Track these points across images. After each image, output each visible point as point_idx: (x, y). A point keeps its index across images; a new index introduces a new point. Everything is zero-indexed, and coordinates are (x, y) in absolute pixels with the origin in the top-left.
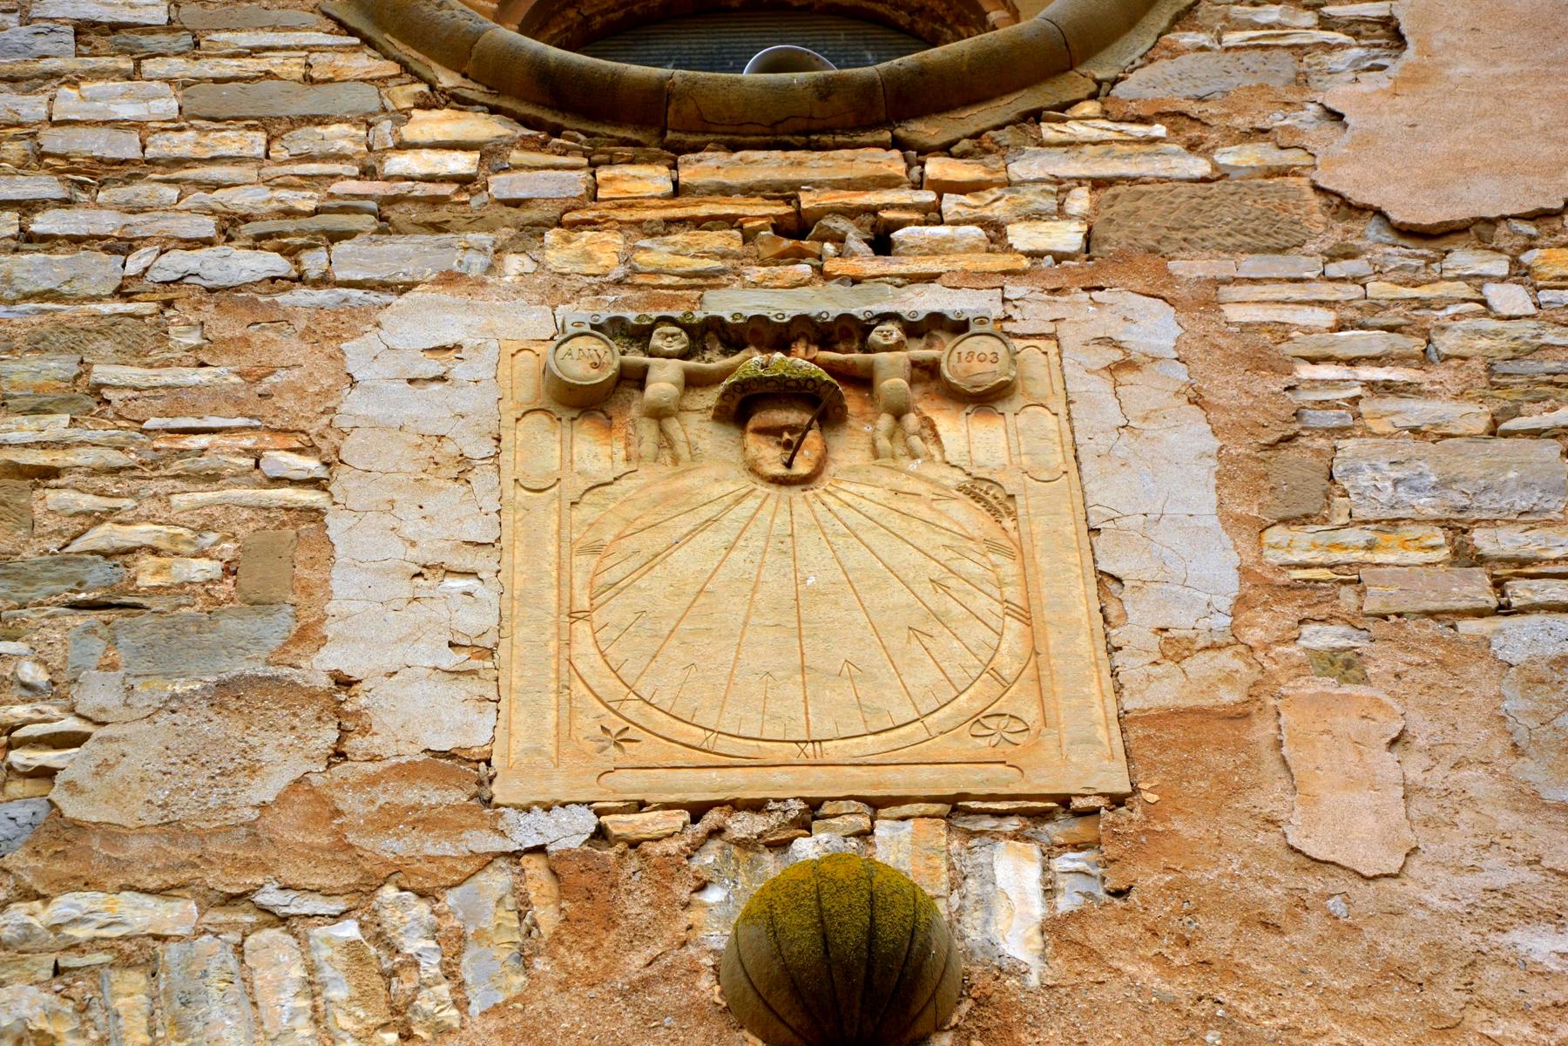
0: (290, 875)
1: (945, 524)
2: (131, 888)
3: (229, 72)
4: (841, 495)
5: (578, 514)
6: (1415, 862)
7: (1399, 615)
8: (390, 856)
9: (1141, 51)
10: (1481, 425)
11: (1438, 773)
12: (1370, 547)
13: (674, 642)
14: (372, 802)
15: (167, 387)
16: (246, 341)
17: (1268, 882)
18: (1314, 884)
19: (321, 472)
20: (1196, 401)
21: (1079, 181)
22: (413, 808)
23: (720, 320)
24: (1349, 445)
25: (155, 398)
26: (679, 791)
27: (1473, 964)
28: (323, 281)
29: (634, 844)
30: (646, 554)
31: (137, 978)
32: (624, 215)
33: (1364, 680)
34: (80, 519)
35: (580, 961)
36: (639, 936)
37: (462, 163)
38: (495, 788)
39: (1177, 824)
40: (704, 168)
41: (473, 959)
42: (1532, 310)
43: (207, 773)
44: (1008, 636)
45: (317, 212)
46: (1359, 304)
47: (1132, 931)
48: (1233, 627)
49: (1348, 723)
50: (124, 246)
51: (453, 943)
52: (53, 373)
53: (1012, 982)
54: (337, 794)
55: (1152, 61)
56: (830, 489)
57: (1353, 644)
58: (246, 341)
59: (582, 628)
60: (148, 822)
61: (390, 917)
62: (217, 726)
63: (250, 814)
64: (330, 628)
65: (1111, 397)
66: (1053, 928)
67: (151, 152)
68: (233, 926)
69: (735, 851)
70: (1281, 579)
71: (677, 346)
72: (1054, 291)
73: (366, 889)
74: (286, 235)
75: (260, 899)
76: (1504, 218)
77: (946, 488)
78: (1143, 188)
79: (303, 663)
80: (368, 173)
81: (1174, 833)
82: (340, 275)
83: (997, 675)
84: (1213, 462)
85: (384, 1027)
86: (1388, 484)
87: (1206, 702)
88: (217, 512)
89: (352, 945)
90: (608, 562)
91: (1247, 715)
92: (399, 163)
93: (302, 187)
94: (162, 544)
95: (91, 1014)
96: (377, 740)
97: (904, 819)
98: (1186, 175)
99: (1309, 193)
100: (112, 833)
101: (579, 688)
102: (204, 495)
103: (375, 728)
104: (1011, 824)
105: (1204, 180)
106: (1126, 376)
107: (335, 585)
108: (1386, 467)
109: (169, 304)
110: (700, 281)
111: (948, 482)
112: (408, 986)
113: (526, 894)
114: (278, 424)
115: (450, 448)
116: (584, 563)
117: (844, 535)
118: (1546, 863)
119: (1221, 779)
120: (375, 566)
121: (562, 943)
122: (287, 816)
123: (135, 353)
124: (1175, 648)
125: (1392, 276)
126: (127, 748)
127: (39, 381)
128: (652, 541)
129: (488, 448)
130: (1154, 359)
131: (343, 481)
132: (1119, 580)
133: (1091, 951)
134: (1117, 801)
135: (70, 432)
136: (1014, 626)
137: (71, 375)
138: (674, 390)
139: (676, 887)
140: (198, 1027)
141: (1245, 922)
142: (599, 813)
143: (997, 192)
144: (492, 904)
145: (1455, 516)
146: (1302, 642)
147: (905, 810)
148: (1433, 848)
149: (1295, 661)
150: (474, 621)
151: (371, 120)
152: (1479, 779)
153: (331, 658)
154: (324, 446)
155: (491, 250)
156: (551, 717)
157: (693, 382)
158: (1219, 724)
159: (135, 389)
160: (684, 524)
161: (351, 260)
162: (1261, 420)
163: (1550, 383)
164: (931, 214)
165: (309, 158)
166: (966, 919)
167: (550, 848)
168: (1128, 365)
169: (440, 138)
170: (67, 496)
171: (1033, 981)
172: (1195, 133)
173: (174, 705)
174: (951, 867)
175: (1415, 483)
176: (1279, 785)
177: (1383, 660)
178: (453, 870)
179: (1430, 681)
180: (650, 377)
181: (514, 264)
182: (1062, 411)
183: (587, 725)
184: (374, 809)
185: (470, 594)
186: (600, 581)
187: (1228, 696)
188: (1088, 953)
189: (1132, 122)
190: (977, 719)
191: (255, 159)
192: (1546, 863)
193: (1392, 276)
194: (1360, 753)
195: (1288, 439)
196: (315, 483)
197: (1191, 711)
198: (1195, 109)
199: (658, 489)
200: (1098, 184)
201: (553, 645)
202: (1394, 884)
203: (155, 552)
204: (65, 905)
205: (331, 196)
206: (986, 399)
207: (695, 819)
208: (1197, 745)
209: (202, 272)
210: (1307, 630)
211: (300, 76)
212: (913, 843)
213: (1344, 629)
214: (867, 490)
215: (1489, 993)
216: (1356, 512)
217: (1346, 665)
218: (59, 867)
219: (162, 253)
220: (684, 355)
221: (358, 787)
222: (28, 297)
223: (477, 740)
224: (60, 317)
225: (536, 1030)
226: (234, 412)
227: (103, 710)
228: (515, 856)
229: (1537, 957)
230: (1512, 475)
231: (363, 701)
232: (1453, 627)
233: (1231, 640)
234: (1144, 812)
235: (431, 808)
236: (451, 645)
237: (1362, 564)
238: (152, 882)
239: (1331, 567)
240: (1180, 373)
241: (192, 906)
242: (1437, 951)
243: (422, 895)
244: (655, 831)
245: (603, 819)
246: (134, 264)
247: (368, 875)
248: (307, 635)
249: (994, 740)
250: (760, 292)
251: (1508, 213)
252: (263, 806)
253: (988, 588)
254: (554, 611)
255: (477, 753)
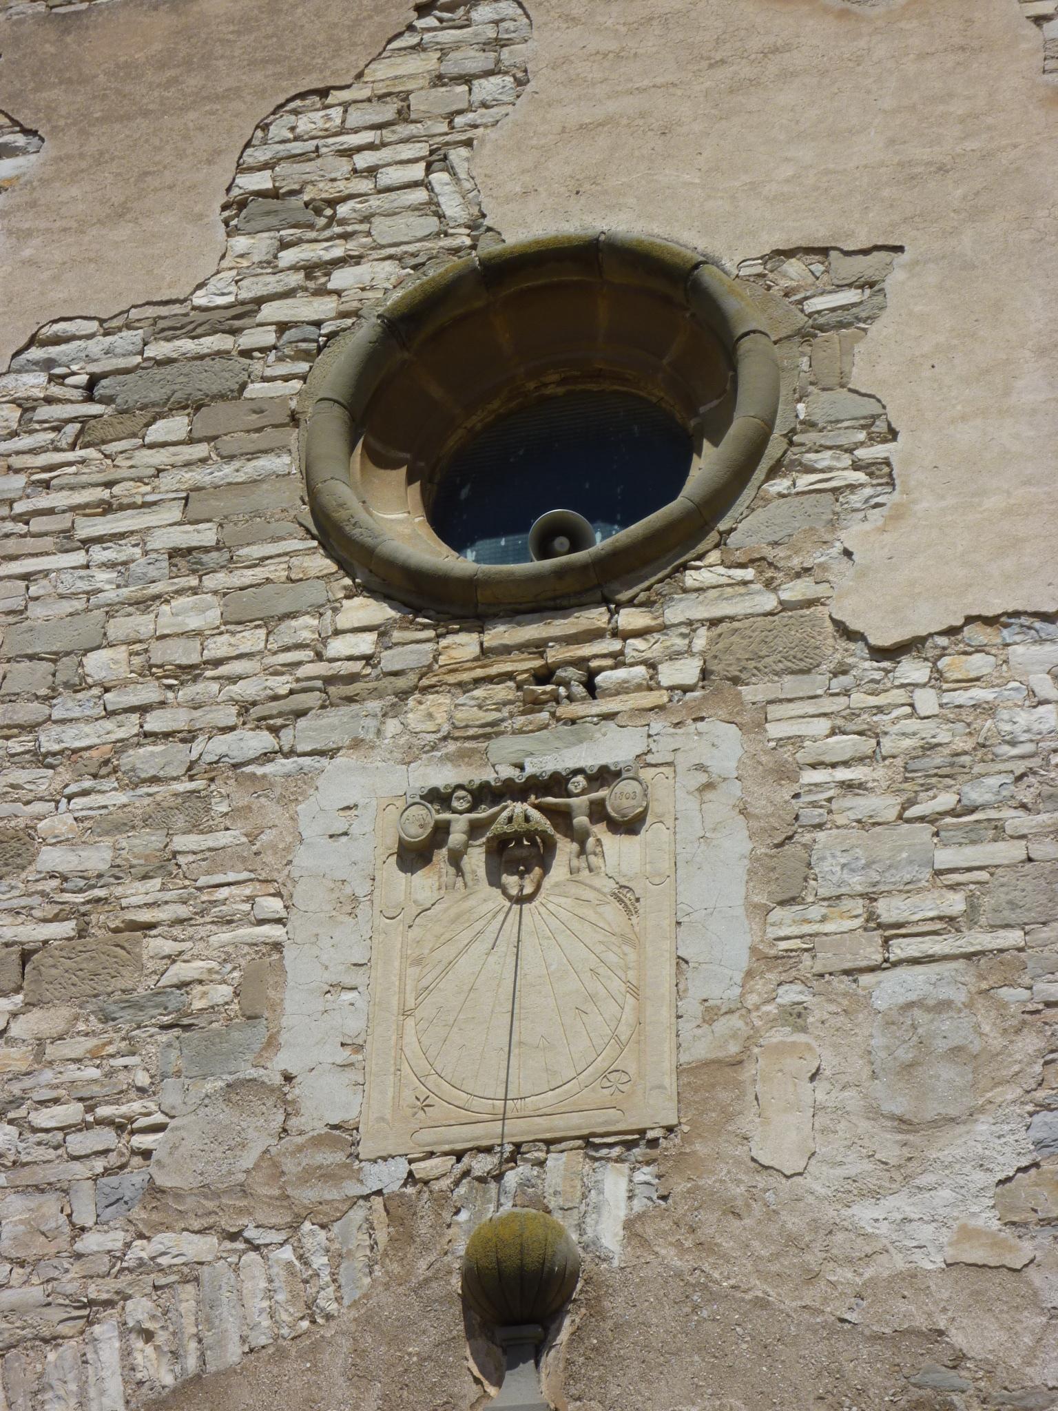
0: (261, 1217)
1: (601, 925)
2: (187, 1230)
3: (247, 581)
4: (550, 906)
5: (411, 934)
6: (813, 1161)
7: (831, 974)
8: (306, 1202)
9: (746, 504)
10: (892, 814)
11: (834, 1094)
12: (824, 919)
13: (455, 1029)
14: (299, 1164)
15: (210, 850)
16: (249, 808)
17: (738, 1182)
18: (761, 1180)
19: (283, 914)
20: (743, 812)
21: (702, 622)
22: (320, 1167)
23: (488, 783)
24: (821, 836)
25: (204, 860)
26: (451, 1142)
27: (830, 1232)
28: (291, 753)
29: (426, 1183)
30: (445, 962)
31: (190, 1288)
32: (451, 679)
33: (804, 1029)
34: (165, 961)
35: (395, 1268)
36: (426, 1248)
37: (365, 644)
38: (360, 1149)
39: (698, 1147)
40: (499, 634)
41: (346, 1269)
42: (936, 710)
43: (222, 1149)
44: (627, 1009)
45: (292, 692)
46: (844, 713)
47: (666, 1225)
48: (742, 995)
49: (791, 1063)
50: (189, 737)
51: (337, 1258)
52: (153, 846)
53: (604, 1266)
54: (283, 1160)
55: (753, 510)
56: (544, 901)
57: (805, 999)
58: (249, 808)
59: (410, 1022)
60: (195, 1185)
61: (308, 1243)
62: (224, 1114)
63: (241, 1177)
64: (283, 1037)
65: (697, 813)
66: (629, 1225)
67: (207, 655)
68: (234, 1251)
69: (476, 1184)
70: (773, 952)
71: (466, 805)
72: (676, 725)
73: (294, 1227)
74: (271, 717)
75: (246, 1234)
76: (931, 635)
77: (604, 895)
78: (736, 624)
79: (269, 1065)
80: (319, 656)
81: (694, 1152)
82: (300, 749)
83: (619, 1042)
84: (746, 862)
85: (302, 1318)
86: (838, 868)
87: (720, 1054)
88: (230, 949)
89: (289, 1264)
90: (425, 971)
91: (741, 1062)
92: (338, 647)
93: (282, 674)
94: (204, 977)
95: (170, 1315)
96: (303, 1120)
97: (562, 1152)
98: (761, 611)
99: (828, 623)
100: (178, 1195)
101: (405, 1067)
102: (225, 935)
103: (302, 1111)
104: (616, 1151)
105: (771, 614)
106: (709, 795)
107: (287, 1004)
108: (839, 854)
109: (212, 780)
110: (488, 730)
111: (606, 890)
112: (314, 1290)
113: (371, 1223)
114: (263, 876)
115: (348, 890)
116: (413, 972)
117: (548, 938)
118: (877, 1156)
119: (723, 1110)
120: (306, 987)
121: (387, 1255)
122: (258, 1177)
123: (195, 827)
124: (711, 1014)
125: (866, 687)
126: (184, 1134)
127: (148, 852)
128: (448, 952)
129: (367, 888)
130: (725, 779)
131: (295, 919)
132: (687, 962)
133: (646, 1240)
134: (670, 1129)
135: (160, 895)
136: (630, 1000)
137: (162, 846)
138: (464, 837)
139: (444, 1214)
140: (217, 1323)
141: (724, 1213)
142: (410, 1162)
143: (656, 635)
144: (355, 1231)
145: (870, 890)
146: (778, 1000)
147: (563, 1146)
148: (824, 1150)
149: (771, 1017)
150: (354, 1025)
151: (321, 610)
152: (852, 1098)
153: (283, 1061)
154: (284, 892)
155: (380, 714)
156: (390, 1095)
157: (475, 829)
158: (727, 1069)
159: (195, 853)
160: (466, 936)
161: (305, 734)
162: (776, 825)
163: (936, 775)
164: (618, 660)
165: (287, 649)
166: (588, 1220)
167: (385, 1191)
168: (709, 786)
169: (356, 625)
170: (159, 941)
171: (616, 1263)
172: (769, 573)
173: (206, 1101)
174: (584, 1185)
175: (853, 866)
176: (753, 1110)
177: (819, 1010)
178: (337, 1209)
179: (839, 1025)
180: (452, 829)
181: (392, 726)
182: (671, 825)
183: (408, 1096)
184: (300, 1169)
185: (352, 1004)
186: (420, 987)
187: (733, 1048)
188: (644, 1243)
189: (736, 567)
190: (605, 1074)
191: (260, 652)
192: (877, 1156)
193: (866, 687)
194: (795, 1085)
195: (790, 838)
196: (279, 921)
197: (713, 1062)
198: (769, 553)
199: (453, 911)
200: (714, 622)
201: (394, 1037)
202: (800, 1178)
203: (200, 982)
204: (162, 1240)
205: (298, 680)
206: (630, 826)
207: (458, 1161)
208: (713, 1086)
209: (230, 753)
210: (781, 990)
211: (283, 579)
212: (566, 1170)
213: (800, 987)
214: (562, 900)
215: (835, 1251)
216: (820, 891)
217: (796, 1016)
218: (155, 1216)
219: (210, 738)
220: (469, 811)
221: (293, 1154)
222: (144, 781)
223: (350, 1115)
224: (158, 798)
225: (372, 1318)
226: (241, 866)
227: (173, 1108)
228: (366, 1198)
229: (862, 1224)
230: (904, 855)
231: (297, 1091)
232: (855, 981)
233: (739, 1005)
234: (682, 1139)
235: (328, 1166)
236: (343, 1045)
237: (817, 935)
238: (196, 1225)
239: (801, 937)
240: (736, 789)
241: (215, 1240)
242: (815, 1225)
243: (323, 1227)
244: (436, 1173)
245: (413, 1166)
246: (197, 747)
247: (297, 1216)
248: (272, 1043)
249: (612, 1089)
250: (521, 738)
251: (932, 631)
252: (247, 1172)
253: (620, 973)
254: (395, 1012)
255: (352, 1124)
